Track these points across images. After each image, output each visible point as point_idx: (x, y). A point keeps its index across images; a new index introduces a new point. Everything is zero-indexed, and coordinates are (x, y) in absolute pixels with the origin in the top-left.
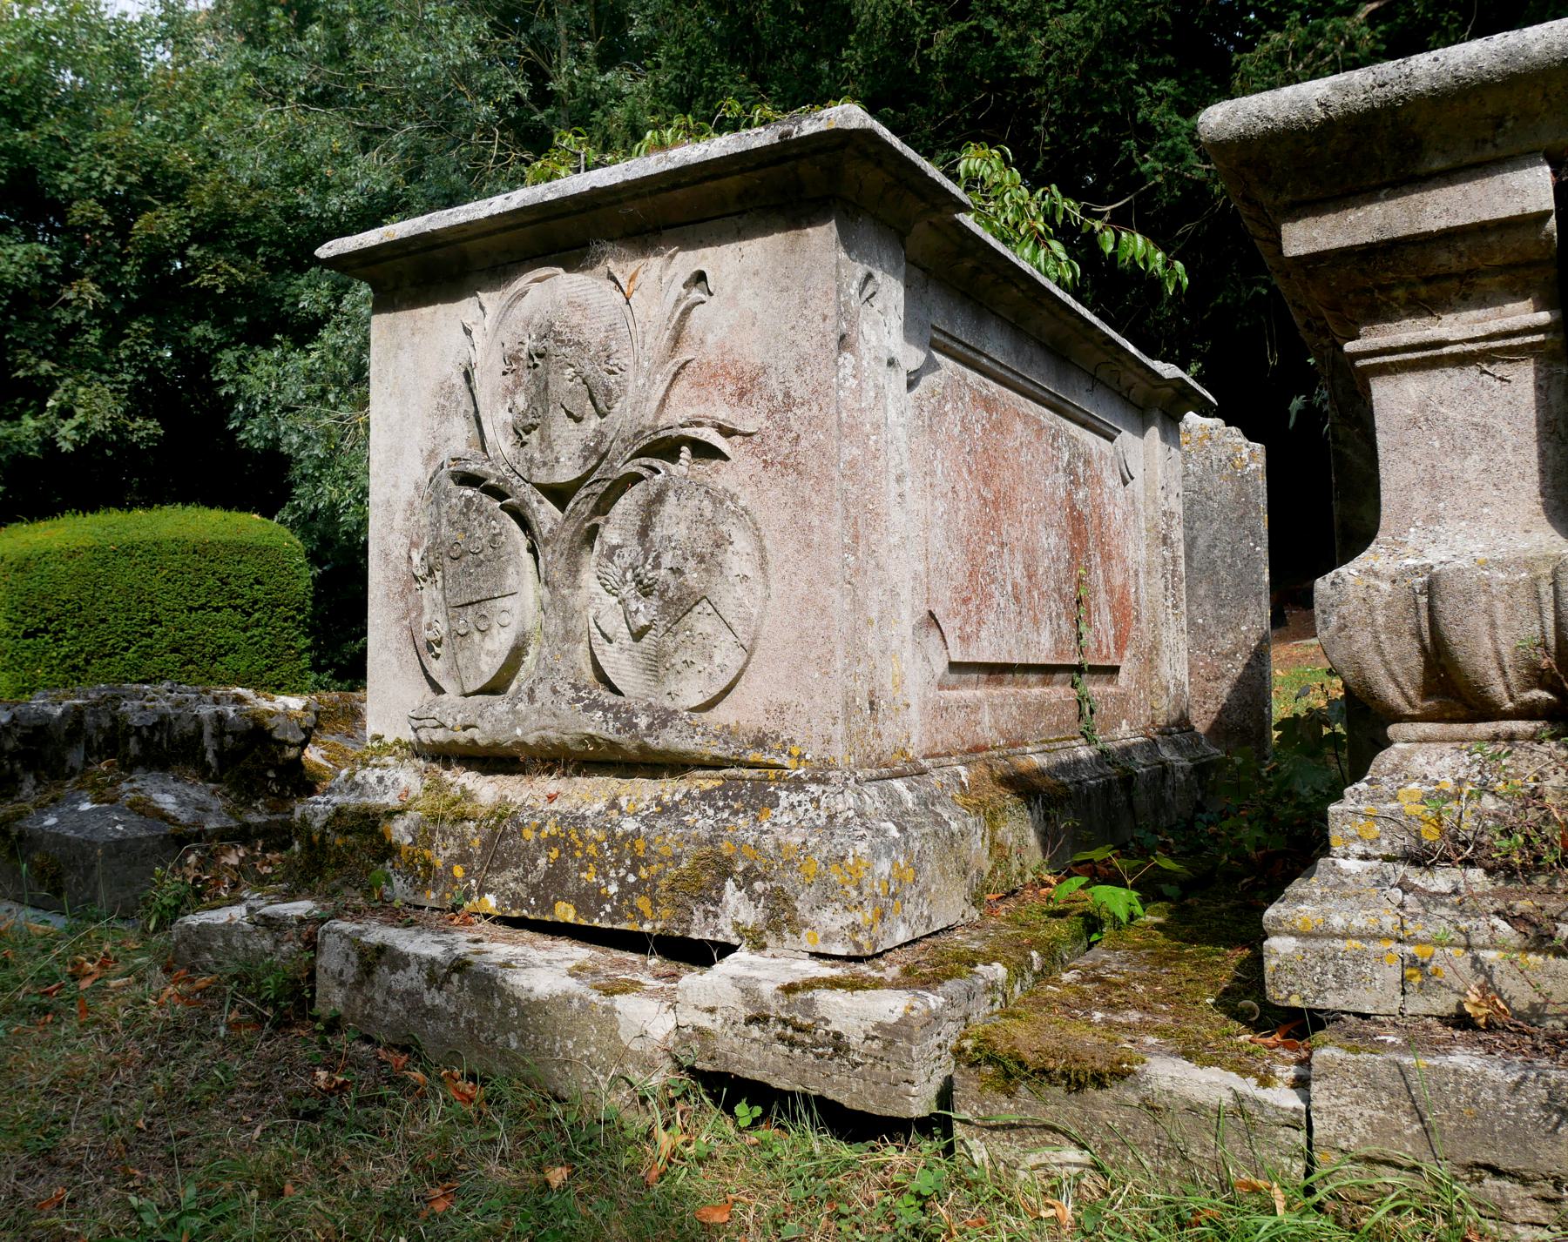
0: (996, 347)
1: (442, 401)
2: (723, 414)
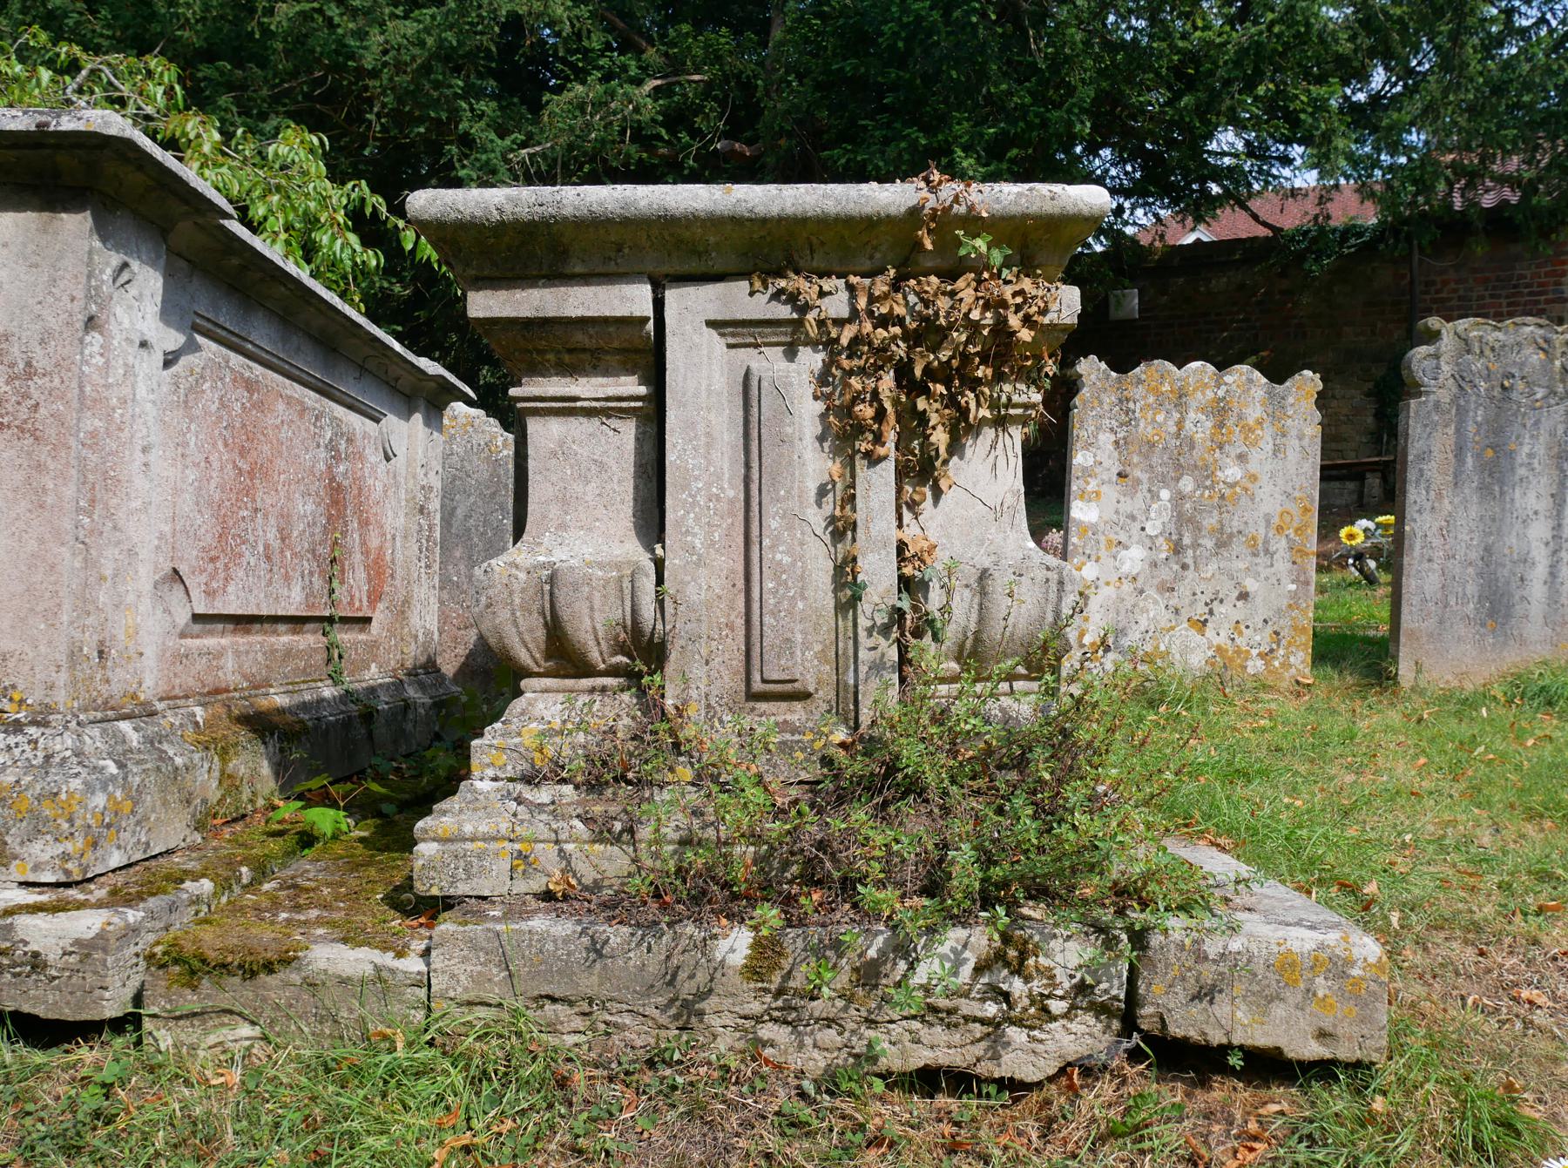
0: (262, 334)
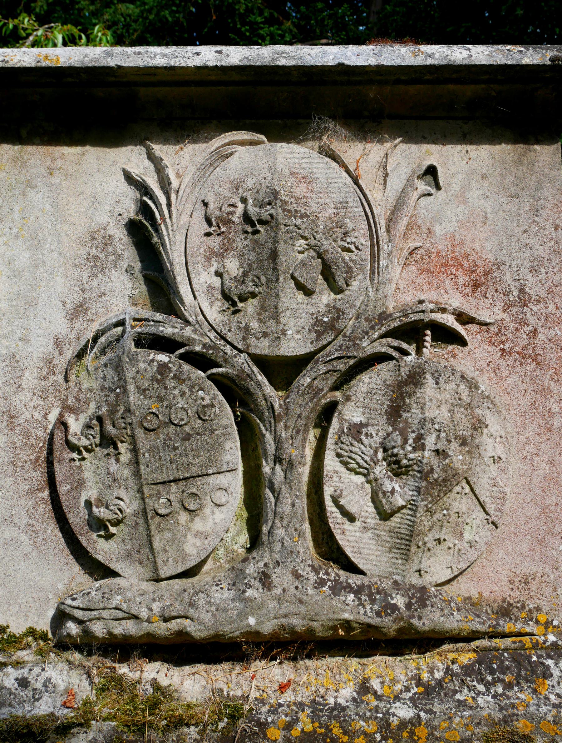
1: (94, 251)
2: (455, 302)
